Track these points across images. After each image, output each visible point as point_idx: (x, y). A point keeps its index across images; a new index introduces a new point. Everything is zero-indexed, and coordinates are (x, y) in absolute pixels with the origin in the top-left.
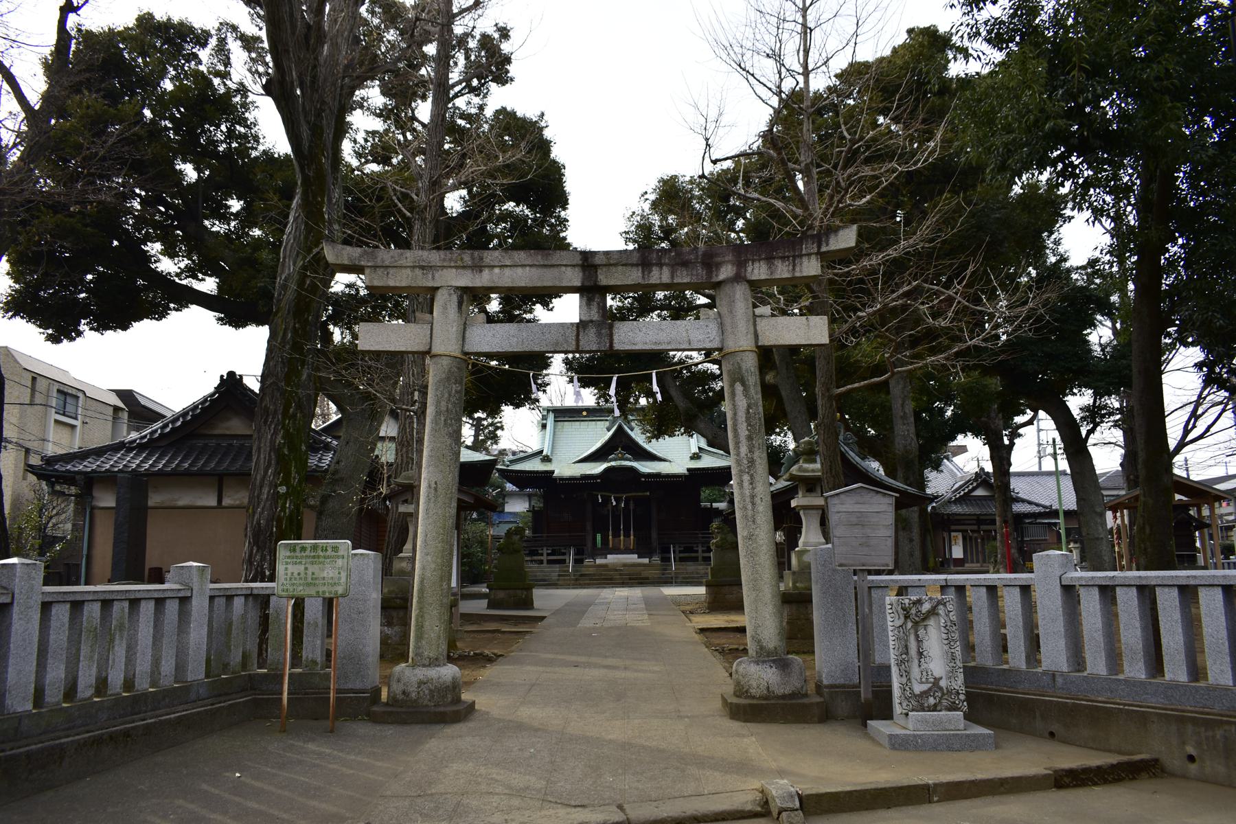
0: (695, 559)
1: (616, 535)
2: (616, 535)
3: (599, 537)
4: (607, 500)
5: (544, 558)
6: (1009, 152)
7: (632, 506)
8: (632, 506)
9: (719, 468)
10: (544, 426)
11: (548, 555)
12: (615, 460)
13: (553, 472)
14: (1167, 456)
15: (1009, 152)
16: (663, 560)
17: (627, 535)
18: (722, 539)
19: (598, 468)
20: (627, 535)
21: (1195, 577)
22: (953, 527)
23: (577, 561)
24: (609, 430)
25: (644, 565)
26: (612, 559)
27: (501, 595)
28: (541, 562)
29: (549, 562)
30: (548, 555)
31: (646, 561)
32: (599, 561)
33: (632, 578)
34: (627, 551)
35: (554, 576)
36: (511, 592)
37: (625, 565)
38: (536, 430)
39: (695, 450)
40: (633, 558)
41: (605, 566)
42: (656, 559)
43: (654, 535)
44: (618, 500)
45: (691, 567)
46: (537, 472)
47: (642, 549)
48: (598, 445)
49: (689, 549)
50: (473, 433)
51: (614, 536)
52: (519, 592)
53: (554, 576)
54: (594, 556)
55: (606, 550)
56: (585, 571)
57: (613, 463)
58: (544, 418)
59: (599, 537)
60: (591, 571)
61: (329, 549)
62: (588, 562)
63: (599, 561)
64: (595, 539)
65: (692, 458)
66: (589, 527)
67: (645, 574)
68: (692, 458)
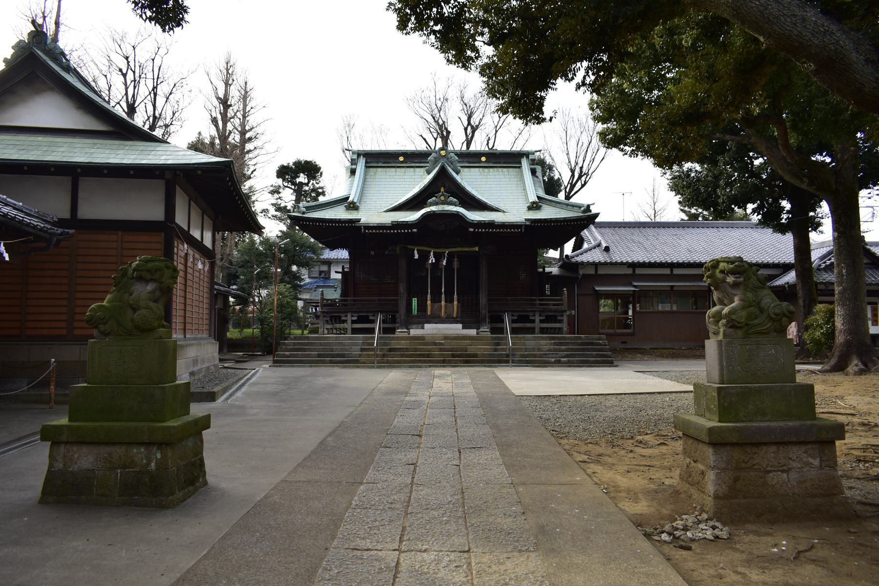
0: (531, 331)
1: (436, 299)
2: (436, 299)
3: (415, 301)
4: (424, 256)
5: (348, 326)
7: (456, 265)
8: (456, 265)
9: (565, 220)
10: (353, 172)
11: (353, 322)
12: (436, 204)
13: (359, 220)
16: (493, 331)
17: (449, 300)
18: (746, 305)
19: (413, 216)
20: (449, 300)
21: (451, 329)
22: (820, 298)
23: (385, 331)
24: (429, 173)
25: (471, 338)
26: (430, 329)
27: (85, 459)
28: (345, 331)
29: (355, 331)
30: (353, 322)
31: (473, 332)
32: (414, 332)
33: (457, 356)
34: (449, 319)
35: (356, 351)
36: (119, 452)
37: (446, 338)
38: (344, 174)
39: (533, 198)
40: (456, 329)
41: (421, 338)
42: (485, 330)
43: (483, 300)
44: (439, 257)
45: (531, 342)
46: (339, 221)
47: (468, 318)
48: (416, 190)
49: (524, 319)
50: (294, 198)
52: (139, 453)
53: (356, 351)
54: (407, 325)
55: (423, 318)
56: (395, 345)
57: (434, 208)
58: (353, 162)
59: (415, 301)
60: (403, 344)
62: (400, 332)
63: (414, 332)
64: (409, 304)
65: (530, 208)
66: (402, 289)
67: (472, 349)
68: (530, 208)
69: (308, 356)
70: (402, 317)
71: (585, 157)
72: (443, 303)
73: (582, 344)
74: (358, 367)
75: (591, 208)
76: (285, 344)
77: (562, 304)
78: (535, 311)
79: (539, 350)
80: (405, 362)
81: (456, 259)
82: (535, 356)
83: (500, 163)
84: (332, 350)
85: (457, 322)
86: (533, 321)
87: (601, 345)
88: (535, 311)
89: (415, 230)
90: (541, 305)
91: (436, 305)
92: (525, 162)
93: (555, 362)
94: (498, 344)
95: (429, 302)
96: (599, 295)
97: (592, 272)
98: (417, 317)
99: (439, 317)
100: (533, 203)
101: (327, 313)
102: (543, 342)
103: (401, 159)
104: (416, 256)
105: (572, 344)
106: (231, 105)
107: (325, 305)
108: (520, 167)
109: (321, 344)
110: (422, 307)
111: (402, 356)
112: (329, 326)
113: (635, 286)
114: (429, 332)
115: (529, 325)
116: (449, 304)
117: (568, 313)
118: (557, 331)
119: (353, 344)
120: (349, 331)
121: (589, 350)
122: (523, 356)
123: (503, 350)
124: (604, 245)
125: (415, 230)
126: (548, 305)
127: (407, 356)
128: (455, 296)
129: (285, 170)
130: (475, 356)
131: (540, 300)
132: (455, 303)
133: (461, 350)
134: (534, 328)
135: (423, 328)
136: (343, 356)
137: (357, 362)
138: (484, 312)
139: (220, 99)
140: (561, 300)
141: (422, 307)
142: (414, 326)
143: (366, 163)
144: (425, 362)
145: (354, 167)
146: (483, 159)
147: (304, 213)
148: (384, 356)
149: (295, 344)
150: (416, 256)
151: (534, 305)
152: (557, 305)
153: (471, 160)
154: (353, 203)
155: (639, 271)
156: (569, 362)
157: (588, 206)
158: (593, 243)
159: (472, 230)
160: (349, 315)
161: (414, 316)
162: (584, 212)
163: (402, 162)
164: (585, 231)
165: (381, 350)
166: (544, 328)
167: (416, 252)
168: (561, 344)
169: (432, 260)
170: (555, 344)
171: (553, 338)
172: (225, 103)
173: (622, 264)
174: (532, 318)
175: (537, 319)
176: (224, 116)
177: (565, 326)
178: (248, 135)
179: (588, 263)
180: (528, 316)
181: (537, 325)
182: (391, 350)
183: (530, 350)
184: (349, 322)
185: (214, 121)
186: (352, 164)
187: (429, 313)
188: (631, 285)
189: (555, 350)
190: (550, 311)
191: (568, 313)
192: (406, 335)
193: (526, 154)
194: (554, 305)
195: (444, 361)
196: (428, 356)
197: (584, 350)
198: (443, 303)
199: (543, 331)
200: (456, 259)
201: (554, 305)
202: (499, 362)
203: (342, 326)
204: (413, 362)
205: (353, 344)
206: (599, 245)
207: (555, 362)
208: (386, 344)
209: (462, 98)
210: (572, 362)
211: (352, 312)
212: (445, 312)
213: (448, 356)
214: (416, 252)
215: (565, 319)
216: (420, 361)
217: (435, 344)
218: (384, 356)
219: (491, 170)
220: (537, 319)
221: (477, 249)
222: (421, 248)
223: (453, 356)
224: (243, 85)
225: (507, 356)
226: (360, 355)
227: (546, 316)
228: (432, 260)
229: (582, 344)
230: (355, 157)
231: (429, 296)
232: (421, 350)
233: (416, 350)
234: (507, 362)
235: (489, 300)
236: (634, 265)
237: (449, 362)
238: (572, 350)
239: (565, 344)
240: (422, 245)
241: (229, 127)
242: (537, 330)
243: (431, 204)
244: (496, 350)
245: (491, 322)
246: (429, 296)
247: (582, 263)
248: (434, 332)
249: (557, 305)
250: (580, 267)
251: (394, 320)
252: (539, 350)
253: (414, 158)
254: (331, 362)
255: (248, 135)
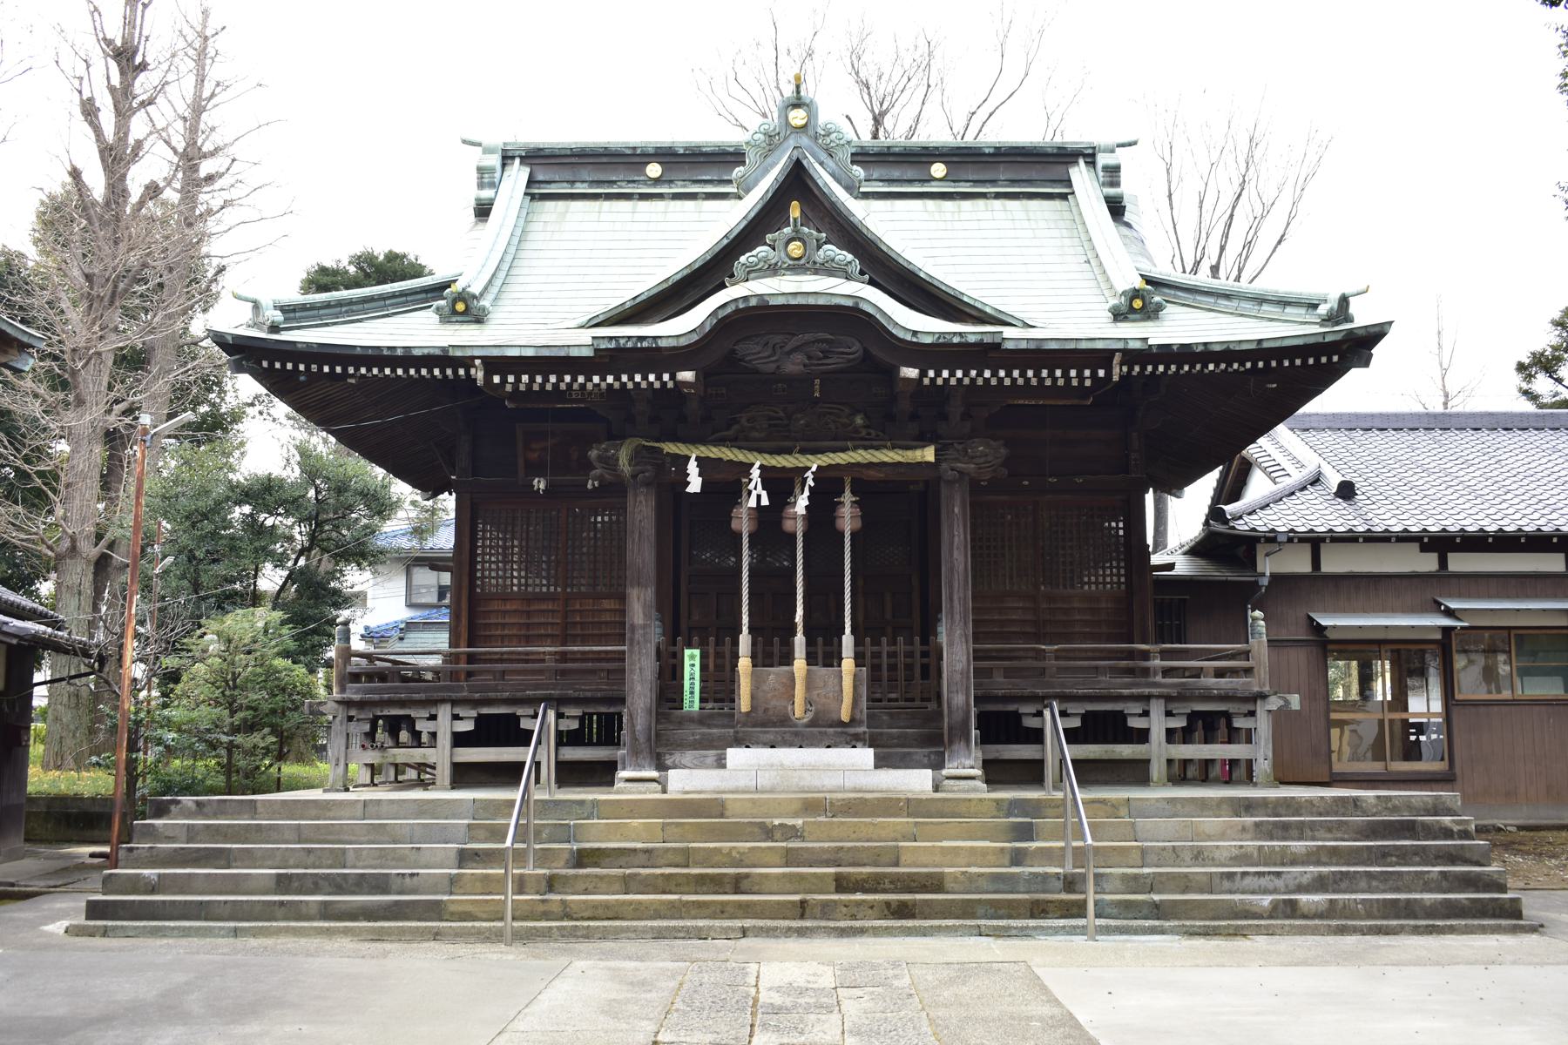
0: (1136, 772)
1: (772, 651)
2: (772, 651)
3: (692, 660)
6: (55, 358)
7: (848, 517)
8: (848, 517)
10: (483, 211)
11: (460, 740)
14: (1145, 554)
15: (55, 358)
16: (995, 773)
21: (829, 768)
25: (913, 806)
26: (749, 768)
30: (460, 740)
31: (916, 781)
32: (687, 780)
34: (826, 730)
37: (812, 806)
40: (850, 768)
41: (707, 807)
43: (955, 649)
46: (407, 358)
47: (903, 719)
51: (761, 658)
54: (659, 754)
55: (725, 725)
56: (600, 835)
58: (485, 177)
59: (692, 660)
60: (634, 834)
61: (908, 648)
62: (633, 783)
64: (670, 674)
65: (1118, 315)
66: (640, 607)
68: (1118, 315)
69: (236, 884)
70: (641, 722)
71: (1226, 235)
72: (800, 664)
73: (1374, 831)
74: (437, 935)
75: (1354, 308)
76: (151, 833)
77: (1248, 671)
78: (1147, 698)
79: (1198, 856)
80: (640, 912)
81: (848, 497)
82: (1185, 884)
83: (993, 182)
84: (339, 858)
85: (853, 741)
86: (1142, 736)
87: (1447, 833)
88: (1147, 698)
89: (687, 376)
90: (1167, 672)
91: (774, 674)
92: (1080, 175)
93: (1276, 911)
94: (1026, 832)
95: (744, 663)
96: (1325, 645)
97: (1302, 565)
98: (702, 720)
99: (784, 721)
100: (1136, 294)
101: (361, 705)
102: (1210, 822)
103: (654, 170)
104: (695, 484)
105: (1329, 828)
106: (143, 67)
107: (355, 677)
108: (1064, 197)
109: (300, 835)
110: (719, 684)
111: (628, 884)
112: (372, 757)
113: (1449, 613)
114: (744, 781)
115: (1125, 751)
116: (821, 671)
117: (1274, 703)
118: (1241, 772)
119: (430, 834)
120: (444, 773)
121: (1404, 856)
122: (1134, 883)
123: (1047, 855)
124: (1333, 480)
125: (687, 376)
126: (1197, 673)
127: (649, 885)
128: (848, 640)
129: (325, 280)
130: (934, 883)
131: (1165, 654)
132: (848, 664)
133: (876, 858)
134: (1145, 763)
135: (721, 763)
136: (380, 884)
137: (435, 910)
138: (959, 699)
139: (109, 42)
140: (1246, 655)
141: (719, 684)
142: (688, 756)
143: (531, 182)
144: (722, 911)
145: (487, 194)
146: (938, 170)
147: (274, 328)
148: (551, 884)
149: (192, 833)
150: (695, 484)
151: (1146, 672)
152: (1234, 672)
153: (896, 173)
154: (462, 296)
155: (1460, 563)
156: (1331, 911)
157: (1344, 301)
158: (1297, 476)
159: (911, 373)
160: (1157, 709)
161: (691, 719)
162: (1331, 319)
163: (657, 181)
164: (1262, 441)
165: (544, 857)
166: (1185, 763)
167: (693, 468)
168: (1284, 831)
169: (757, 494)
170: (1261, 831)
171: (1248, 806)
172: (126, 57)
173: (1405, 538)
174: (1134, 723)
175: (1158, 724)
176: (124, 101)
177: (1261, 753)
178: (206, 168)
179: (1294, 538)
180: (1121, 717)
181: (1158, 750)
182: (582, 858)
183: (1161, 856)
184: (445, 740)
185: (89, 111)
186: (481, 186)
187: (744, 704)
188: (1437, 607)
189: (1265, 857)
190: (1207, 697)
191: (1274, 703)
192: (651, 793)
193: (1089, 156)
194: (1220, 673)
195: (802, 910)
196: (737, 884)
197: (1383, 856)
198: (800, 664)
199: (1181, 773)
200: (848, 497)
201: (1220, 673)
202: (1038, 910)
203: (417, 755)
204: (676, 911)
205: (430, 834)
206: (1316, 480)
207: (1276, 911)
208: (566, 834)
209: (856, 55)
210: (1346, 911)
211: (454, 703)
212: (809, 702)
213: (817, 884)
214: (693, 468)
215: (1263, 725)
216: (701, 909)
217: (768, 833)
218: (551, 884)
219: (966, 205)
220: (1158, 724)
221: (929, 454)
222: (714, 452)
223: (842, 884)
224: (196, 20)
225: (1070, 883)
226: (453, 883)
227: (1193, 717)
228: (757, 494)
229: (1374, 831)
230: (495, 161)
231: (745, 640)
232: (708, 858)
233: (687, 858)
234: (1078, 910)
235: (978, 656)
236: (1441, 544)
237: (827, 911)
238: (1335, 854)
239: (1301, 831)
240: (719, 442)
241: (138, 127)
242: (1157, 770)
243: (751, 273)
244: (1018, 858)
245: (985, 740)
246: (745, 640)
247: (1271, 538)
248: (765, 780)
249: (1234, 672)
250: (1261, 550)
251: (609, 732)
252: (1198, 856)
253: (697, 167)
254: (327, 912)
255: (206, 168)
